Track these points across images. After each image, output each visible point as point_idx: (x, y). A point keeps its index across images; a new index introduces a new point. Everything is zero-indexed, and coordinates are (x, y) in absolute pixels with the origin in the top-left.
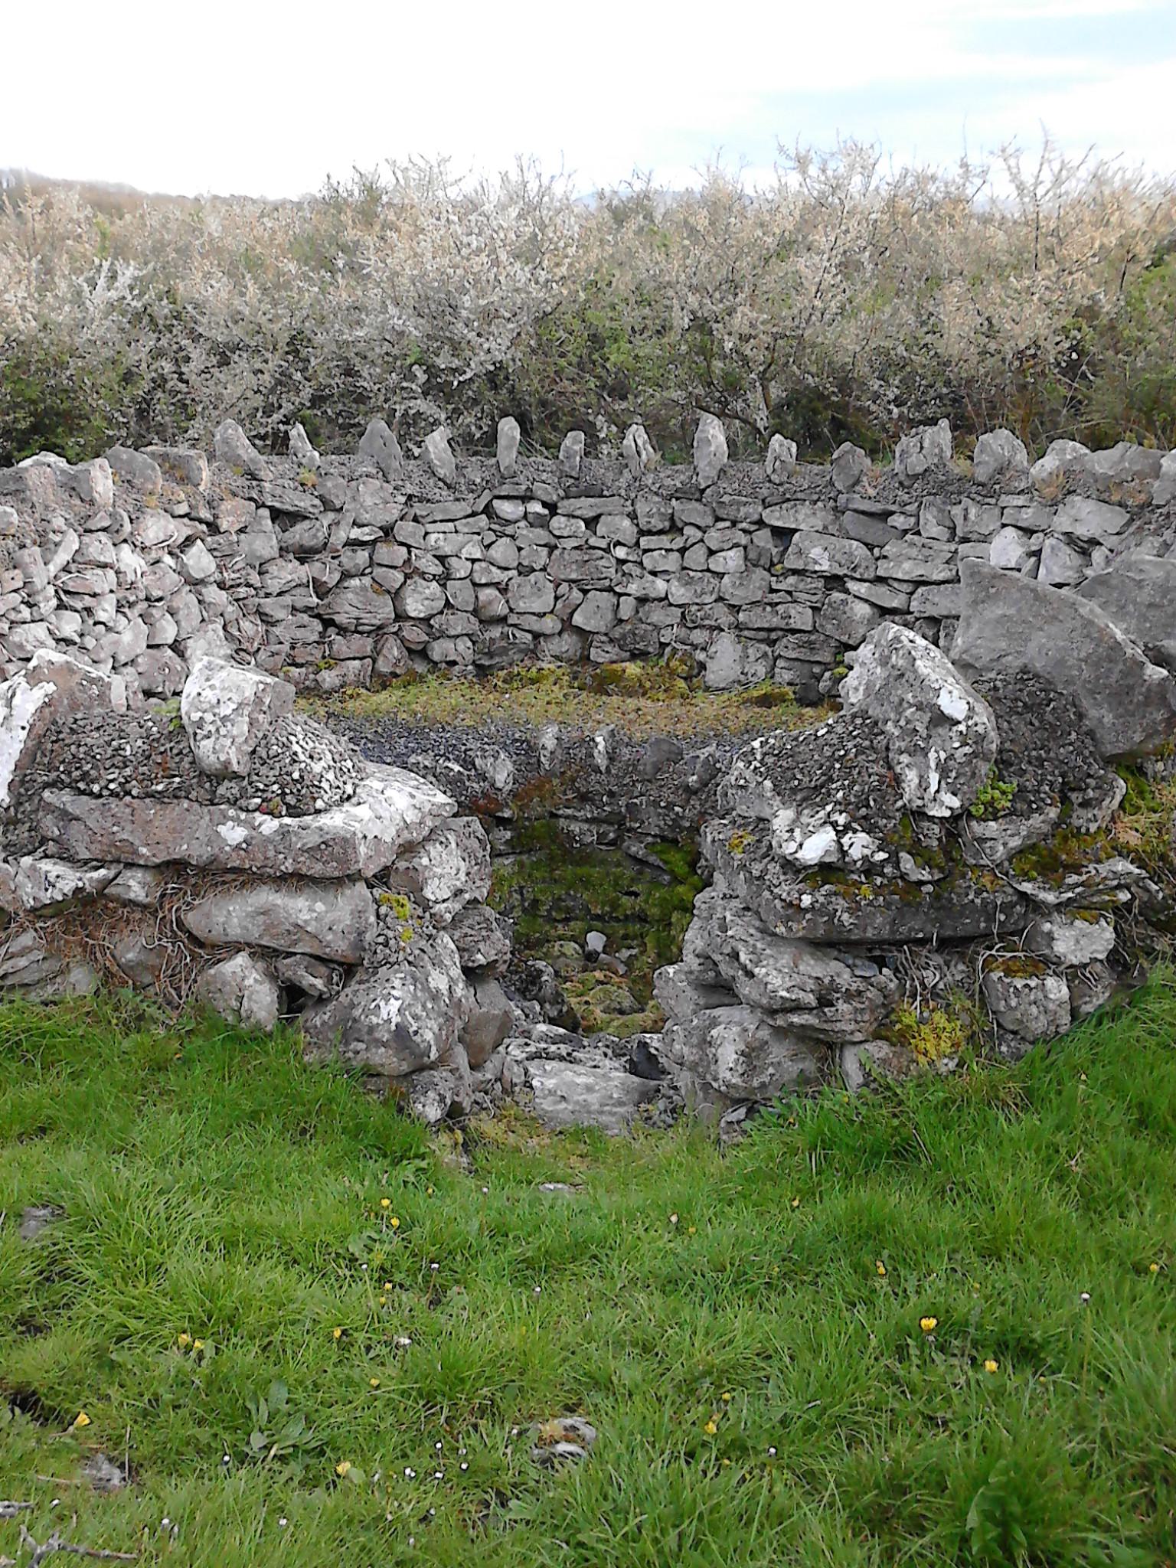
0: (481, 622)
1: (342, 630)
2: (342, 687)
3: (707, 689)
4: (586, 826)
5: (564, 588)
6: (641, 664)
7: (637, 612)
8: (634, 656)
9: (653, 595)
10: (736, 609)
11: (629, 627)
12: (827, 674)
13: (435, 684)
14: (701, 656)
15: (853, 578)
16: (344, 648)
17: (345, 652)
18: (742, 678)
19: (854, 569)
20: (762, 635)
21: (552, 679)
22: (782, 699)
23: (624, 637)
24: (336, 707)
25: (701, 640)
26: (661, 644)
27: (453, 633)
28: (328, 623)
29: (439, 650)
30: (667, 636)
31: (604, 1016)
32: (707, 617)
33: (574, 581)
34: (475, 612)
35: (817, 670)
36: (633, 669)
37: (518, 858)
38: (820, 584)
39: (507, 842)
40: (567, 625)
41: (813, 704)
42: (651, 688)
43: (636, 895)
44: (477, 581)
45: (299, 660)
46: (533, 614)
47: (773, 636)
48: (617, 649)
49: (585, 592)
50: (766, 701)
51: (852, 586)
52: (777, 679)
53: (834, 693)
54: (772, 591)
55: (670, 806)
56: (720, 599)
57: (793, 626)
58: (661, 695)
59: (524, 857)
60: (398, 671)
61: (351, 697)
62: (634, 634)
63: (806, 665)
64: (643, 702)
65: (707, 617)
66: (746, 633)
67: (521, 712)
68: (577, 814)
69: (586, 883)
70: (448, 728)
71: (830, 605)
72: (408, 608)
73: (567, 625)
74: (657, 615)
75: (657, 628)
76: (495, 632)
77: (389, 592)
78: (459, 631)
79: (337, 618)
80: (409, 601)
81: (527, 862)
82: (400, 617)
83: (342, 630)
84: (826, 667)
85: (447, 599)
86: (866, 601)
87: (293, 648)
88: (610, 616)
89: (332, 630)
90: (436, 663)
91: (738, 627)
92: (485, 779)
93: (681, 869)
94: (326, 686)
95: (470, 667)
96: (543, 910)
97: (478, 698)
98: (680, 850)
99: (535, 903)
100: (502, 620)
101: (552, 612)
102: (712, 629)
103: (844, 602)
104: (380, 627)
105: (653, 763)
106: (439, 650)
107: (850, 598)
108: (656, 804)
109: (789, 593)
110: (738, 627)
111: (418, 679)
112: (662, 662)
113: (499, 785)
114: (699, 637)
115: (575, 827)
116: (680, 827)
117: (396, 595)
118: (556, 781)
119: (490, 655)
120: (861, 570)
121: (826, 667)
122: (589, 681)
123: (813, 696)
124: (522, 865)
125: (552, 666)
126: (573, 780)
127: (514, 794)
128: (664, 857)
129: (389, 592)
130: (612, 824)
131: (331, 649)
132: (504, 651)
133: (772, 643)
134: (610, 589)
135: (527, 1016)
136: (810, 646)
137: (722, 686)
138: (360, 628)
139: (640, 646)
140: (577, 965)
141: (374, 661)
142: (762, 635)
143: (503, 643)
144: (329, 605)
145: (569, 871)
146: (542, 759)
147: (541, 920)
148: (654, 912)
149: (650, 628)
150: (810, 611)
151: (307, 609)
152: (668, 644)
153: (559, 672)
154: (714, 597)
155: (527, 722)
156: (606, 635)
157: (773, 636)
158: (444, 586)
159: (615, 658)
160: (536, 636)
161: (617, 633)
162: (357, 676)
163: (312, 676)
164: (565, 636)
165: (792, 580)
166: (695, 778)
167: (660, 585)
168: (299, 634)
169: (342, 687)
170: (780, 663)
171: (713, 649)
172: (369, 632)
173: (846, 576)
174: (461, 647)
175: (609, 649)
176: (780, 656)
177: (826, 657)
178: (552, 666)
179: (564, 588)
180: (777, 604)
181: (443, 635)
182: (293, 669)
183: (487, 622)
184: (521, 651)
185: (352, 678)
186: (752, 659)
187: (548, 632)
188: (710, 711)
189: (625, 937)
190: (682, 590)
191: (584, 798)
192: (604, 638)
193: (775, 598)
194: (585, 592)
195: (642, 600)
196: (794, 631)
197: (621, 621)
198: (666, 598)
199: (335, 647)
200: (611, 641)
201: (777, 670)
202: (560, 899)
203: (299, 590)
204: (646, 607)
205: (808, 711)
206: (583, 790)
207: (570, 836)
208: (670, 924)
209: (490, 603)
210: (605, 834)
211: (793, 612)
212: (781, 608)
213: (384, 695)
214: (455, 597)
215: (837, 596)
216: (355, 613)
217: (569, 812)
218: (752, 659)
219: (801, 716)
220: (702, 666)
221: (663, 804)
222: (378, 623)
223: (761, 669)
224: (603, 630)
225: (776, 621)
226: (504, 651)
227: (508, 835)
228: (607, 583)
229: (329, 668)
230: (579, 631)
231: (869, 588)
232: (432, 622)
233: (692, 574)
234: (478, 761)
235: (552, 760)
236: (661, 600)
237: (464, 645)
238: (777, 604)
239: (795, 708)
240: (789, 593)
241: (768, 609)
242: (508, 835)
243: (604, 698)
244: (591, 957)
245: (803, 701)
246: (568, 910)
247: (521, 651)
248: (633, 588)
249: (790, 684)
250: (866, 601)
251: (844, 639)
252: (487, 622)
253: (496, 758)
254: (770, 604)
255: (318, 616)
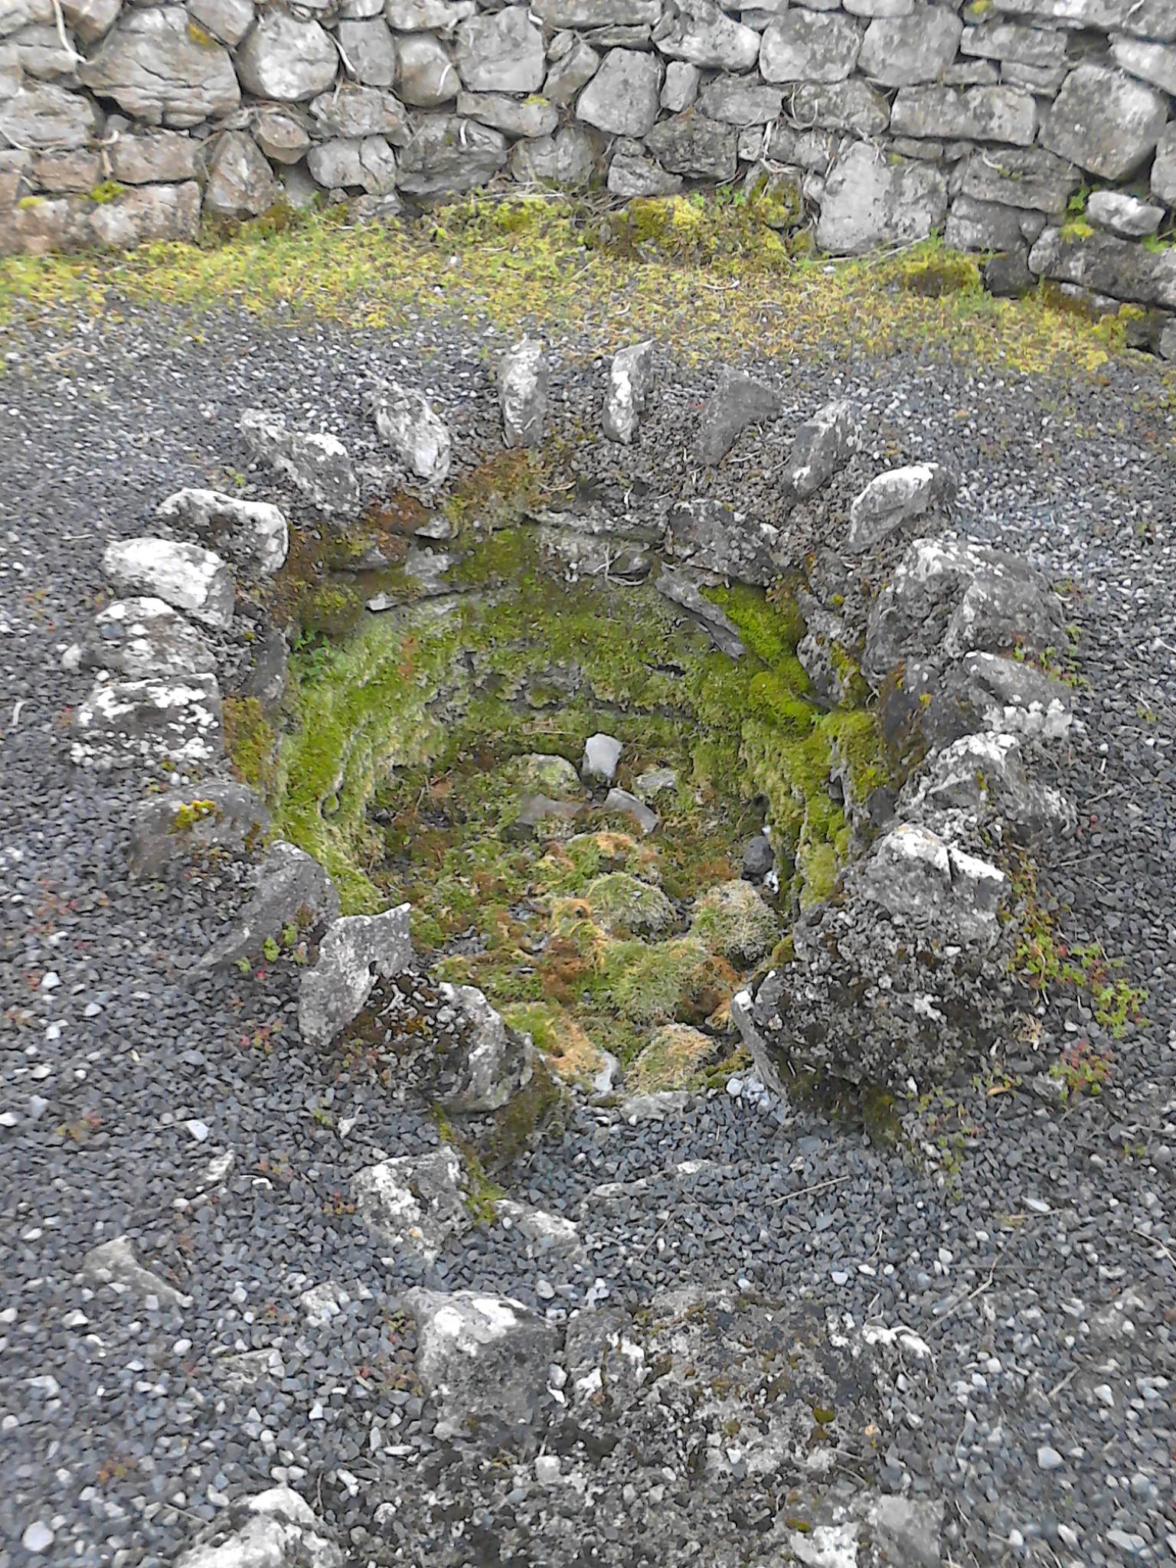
0: (409, 108)
1: (136, 122)
2: (141, 239)
3: (819, 251)
4: (589, 544)
5: (562, 42)
6: (701, 200)
7: (699, 94)
8: (690, 183)
9: (730, 62)
10: (889, 95)
11: (681, 127)
12: (1048, 235)
13: (320, 234)
14: (812, 188)
15: (1129, 35)
16: (139, 162)
17: (142, 169)
18: (886, 233)
19: (1136, 16)
20: (934, 149)
21: (538, 224)
22: (958, 281)
23: (672, 145)
24: (127, 281)
25: (815, 157)
26: (740, 161)
27: (354, 130)
28: (108, 106)
29: (331, 163)
30: (752, 147)
31: (614, 945)
32: (830, 110)
33: (582, 29)
34: (396, 89)
35: (1028, 225)
36: (686, 210)
37: (463, 601)
38: (1061, 44)
39: (440, 576)
40: (567, 119)
41: (1015, 294)
42: (720, 250)
43: (678, 671)
44: (398, 23)
45: (50, 184)
46: (506, 94)
47: (953, 153)
48: (657, 170)
49: (602, 51)
50: (929, 284)
51: (1126, 52)
52: (952, 238)
53: (1058, 273)
54: (961, 57)
55: (751, 524)
56: (859, 72)
57: (996, 135)
58: (737, 266)
59: (474, 599)
60: (251, 207)
61: (160, 262)
62: (692, 142)
63: (1009, 213)
64: (702, 278)
65: (830, 110)
66: (902, 145)
67: (477, 299)
68: (573, 523)
69: (586, 644)
70: (336, 334)
71: (1073, 90)
72: (264, 77)
73: (567, 119)
74: (737, 104)
75: (735, 129)
76: (436, 129)
77: (223, 44)
78: (366, 125)
79: (122, 97)
80: (266, 63)
81: (481, 608)
82: (251, 94)
83: (136, 122)
84: (1047, 219)
85: (341, 62)
86: (1151, 86)
87: (37, 158)
88: (646, 102)
89: (115, 119)
90: (323, 189)
91: (889, 133)
92: (395, 457)
93: (771, 646)
94: (110, 237)
95: (390, 198)
96: (510, 692)
97: (402, 263)
98: (765, 607)
99: (495, 680)
100: (449, 104)
101: (540, 90)
102: (838, 134)
103: (1104, 87)
104: (212, 118)
105: (723, 432)
106: (331, 163)
107: (1117, 79)
108: (725, 516)
109: (996, 64)
110: (889, 133)
111: (288, 222)
112: (740, 199)
113: (423, 469)
114: (811, 149)
115: (570, 546)
116: (769, 564)
117: (240, 51)
118: (534, 458)
119: (427, 174)
120: (1149, 17)
121: (1047, 219)
122: (604, 231)
123: (1016, 277)
124: (469, 613)
125: (538, 199)
126: (568, 457)
127: (452, 485)
128: (736, 615)
129: (223, 44)
130: (641, 542)
131: (114, 163)
132: (453, 167)
133: (948, 166)
134: (651, 48)
135: (424, 1205)
136: (1025, 178)
137: (847, 246)
138: (172, 119)
139: (703, 165)
140: (565, 810)
141: (205, 186)
142: (934, 149)
143: (450, 153)
144: (100, 69)
145: (554, 625)
146: (509, 414)
147: (506, 707)
148: (711, 712)
149: (721, 129)
150: (1031, 103)
151: (58, 77)
152: (752, 163)
153: (552, 210)
154: (847, 68)
155: (485, 323)
156: (639, 139)
157: (953, 153)
158: (334, 32)
159: (654, 187)
160: (512, 139)
161: (659, 138)
162: (171, 217)
163: (80, 217)
164: (565, 139)
165: (1003, 34)
166: (806, 471)
167: (746, 39)
168: (47, 128)
169: (141, 239)
170: (960, 208)
171: (836, 176)
172: (192, 129)
173: (1116, 28)
174: (371, 159)
175: (643, 170)
176: (961, 193)
177: (1052, 200)
178: (538, 199)
179: (562, 42)
180: (969, 86)
181: (336, 135)
182: (41, 202)
183: (418, 108)
184: (482, 167)
185: (160, 220)
186: (908, 197)
187: (531, 133)
188: (828, 302)
189: (655, 743)
190: (788, 53)
191: (588, 491)
192: (636, 148)
193: (966, 73)
194: (602, 51)
195: (710, 71)
196: (993, 145)
197: (670, 113)
198: (756, 66)
199: (121, 158)
200: (648, 152)
201: (952, 221)
202: (539, 673)
203: (36, 35)
204: (717, 85)
205: (1005, 307)
206: (587, 475)
207: (561, 562)
208: (740, 739)
209: (423, 69)
210: (626, 559)
211: (998, 106)
212: (975, 96)
213: (226, 255)
214: (356, 56)
215: (1089, 72)
216: (158, 87)
217: (559, 518)
218: (908, 197)
219: (995, 320)
220: (813, 207)
221: (738, 517)
222: (209, 108)
223: (923, 219)
224: (634, 129)
225: (962, 123)
226: (453, 167)
227: (443, 562)
228: (644, 32)
229: (116, 200)
230: (589, 129)
231: (1162, 58)
232: (314, 108)
233: (808, 17)
234: (381, 419)
235: (525, 415)
236: (745, 71)
237: (377, 155)
238: (969, 86)
239: (982, 301)
240: (996, 64)
241: (951, 96)
242: (443, 562)
243: (631, 267)
244: (595, 786)
245: (995, 287)
246: (556, 692)
247: (482, 167)
248: (694, 46)
249: (974, 249)
250: (1151, 86)
251: (1094, 165)
252: (418, 108)
253: (416, 418)
254: (955, 87)
255: (83, 90)
